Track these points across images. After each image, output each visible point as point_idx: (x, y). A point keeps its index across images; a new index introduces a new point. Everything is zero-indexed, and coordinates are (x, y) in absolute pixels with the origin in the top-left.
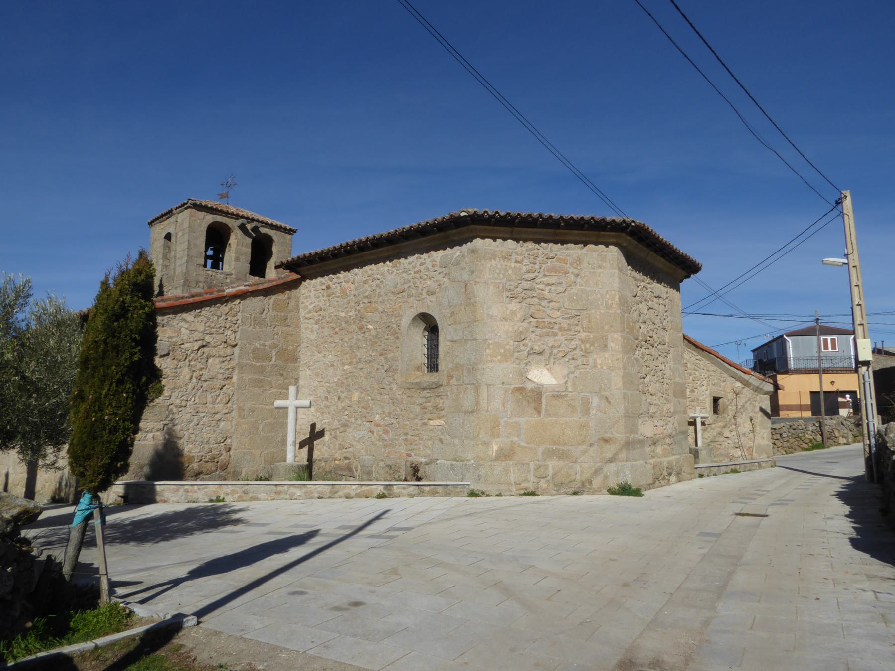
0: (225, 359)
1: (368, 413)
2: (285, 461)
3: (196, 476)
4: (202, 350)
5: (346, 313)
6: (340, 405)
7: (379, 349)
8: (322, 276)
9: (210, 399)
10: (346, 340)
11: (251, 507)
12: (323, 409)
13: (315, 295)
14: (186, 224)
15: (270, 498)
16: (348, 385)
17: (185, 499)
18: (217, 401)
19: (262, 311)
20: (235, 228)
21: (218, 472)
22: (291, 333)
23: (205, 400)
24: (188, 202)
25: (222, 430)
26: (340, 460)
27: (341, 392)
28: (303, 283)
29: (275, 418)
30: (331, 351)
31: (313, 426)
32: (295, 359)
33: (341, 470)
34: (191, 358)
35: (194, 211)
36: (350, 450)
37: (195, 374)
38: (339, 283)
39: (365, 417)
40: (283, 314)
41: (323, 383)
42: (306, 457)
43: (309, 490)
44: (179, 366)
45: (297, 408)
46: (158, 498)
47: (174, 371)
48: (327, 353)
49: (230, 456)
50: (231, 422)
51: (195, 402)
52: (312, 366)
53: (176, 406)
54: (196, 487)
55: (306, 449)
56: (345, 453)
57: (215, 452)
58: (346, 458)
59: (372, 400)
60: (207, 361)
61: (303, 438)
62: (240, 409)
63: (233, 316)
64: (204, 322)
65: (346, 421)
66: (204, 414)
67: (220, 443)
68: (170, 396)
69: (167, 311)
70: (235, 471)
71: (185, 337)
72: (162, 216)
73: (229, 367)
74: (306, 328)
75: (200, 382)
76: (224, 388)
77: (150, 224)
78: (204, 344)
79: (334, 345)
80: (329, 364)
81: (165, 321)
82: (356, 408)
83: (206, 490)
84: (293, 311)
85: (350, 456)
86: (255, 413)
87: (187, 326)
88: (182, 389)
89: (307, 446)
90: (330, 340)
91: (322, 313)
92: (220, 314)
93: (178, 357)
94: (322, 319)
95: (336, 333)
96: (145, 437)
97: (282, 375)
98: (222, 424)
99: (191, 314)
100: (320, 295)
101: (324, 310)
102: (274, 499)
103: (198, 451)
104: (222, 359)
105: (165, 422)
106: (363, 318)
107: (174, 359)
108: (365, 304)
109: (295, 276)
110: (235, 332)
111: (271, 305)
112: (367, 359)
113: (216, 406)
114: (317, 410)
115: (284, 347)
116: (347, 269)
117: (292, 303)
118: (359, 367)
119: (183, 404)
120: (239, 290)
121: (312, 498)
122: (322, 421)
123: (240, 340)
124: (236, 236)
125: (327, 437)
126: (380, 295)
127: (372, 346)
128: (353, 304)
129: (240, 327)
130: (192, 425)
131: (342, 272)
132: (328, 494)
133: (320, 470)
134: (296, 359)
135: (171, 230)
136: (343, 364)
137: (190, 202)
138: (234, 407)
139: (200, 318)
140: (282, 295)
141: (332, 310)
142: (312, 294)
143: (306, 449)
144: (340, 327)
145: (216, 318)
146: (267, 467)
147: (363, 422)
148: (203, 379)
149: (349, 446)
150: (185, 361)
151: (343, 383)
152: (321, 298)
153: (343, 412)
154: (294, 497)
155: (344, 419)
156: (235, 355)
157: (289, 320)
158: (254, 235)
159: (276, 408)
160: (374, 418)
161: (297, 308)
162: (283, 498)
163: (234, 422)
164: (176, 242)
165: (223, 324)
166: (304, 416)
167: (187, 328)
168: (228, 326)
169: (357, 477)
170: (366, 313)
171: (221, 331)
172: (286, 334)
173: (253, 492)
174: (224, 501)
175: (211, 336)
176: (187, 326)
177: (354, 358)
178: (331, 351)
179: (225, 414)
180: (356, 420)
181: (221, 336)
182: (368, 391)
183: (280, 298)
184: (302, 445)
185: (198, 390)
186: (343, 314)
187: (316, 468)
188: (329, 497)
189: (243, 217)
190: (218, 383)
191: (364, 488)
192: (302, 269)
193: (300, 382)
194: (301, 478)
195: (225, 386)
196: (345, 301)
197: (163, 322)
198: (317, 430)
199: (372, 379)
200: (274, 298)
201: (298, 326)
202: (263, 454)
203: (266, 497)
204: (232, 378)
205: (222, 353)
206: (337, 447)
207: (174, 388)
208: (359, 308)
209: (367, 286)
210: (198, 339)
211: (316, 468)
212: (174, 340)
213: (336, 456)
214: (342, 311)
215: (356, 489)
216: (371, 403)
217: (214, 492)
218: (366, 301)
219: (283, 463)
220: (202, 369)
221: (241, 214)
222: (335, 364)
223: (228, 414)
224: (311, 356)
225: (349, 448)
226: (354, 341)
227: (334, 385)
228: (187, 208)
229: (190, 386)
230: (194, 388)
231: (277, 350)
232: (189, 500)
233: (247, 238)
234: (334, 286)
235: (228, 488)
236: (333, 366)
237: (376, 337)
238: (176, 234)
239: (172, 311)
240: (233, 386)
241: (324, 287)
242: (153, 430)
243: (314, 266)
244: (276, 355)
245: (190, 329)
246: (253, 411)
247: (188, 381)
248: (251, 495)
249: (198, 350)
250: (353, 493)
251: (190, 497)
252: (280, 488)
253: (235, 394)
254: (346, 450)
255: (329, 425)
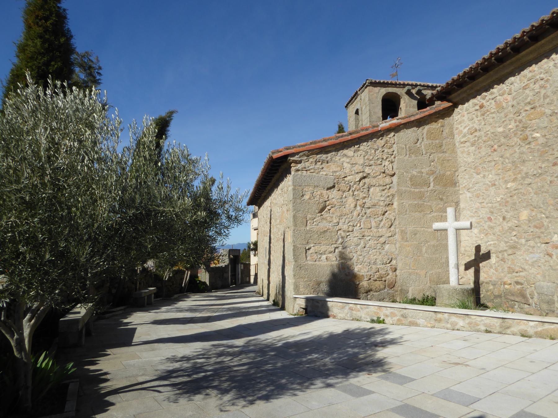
0: (385, 187)
1: (542, 233)
2: (448, 282)
3: (367, 293)
4: (363, 181)
5: (504, 128)
6: (506, 225)
7: (551, 158)
8: (475, 97)
9: (373, 224)
10: (508, 155)
11: (405, 338)
12: (487, 230)
13: (469, 118)
14: (367, 99)
15: (429, 325)
16: (514, 204)
17: (350, 317)
18: (381, 225)
19: (416, 140)
20: (403, 95)
21: (386, 290)
22: (447, 158)
23: (369, 225)
24: (366, 82)
25: (387, 252)
26: (511, 284)
27: (506, 211)
28: (456, 110)
29: (438, 240)
30: (491, 170)
31: (478, 248)
32: (454, 184)
33: (513, 295)
34: (354, 189)
35: (371, 87)
36: (521, 274)
37: (359, 203)
38: (493, 99)
39: (539, 237)
40: (437, 141)
41: (485, 204)
42: (472, 279)
43: (474, 321)
44: (344, 196)
45: (457, 230)
46: (330, 313)
47: (339, 200)
48: (487, 174)
49: (396, 276)
50: (395, 244)
51: (361, 227)
52: (472, 188)
53: (344, 231)
54: (358, 306)
55: (472, 270)
56: (516, 277)
57: (382, 272)
58: (517, 283)
59: (547, 217)
60: (369, 191)
61: (468, 259)
62: (403, 232)
63: (389, 148)
64: (362, 156)
65: (515, 242)
66: (369, 238)
67: (386, 264)
68: (338, 223)
69: (330, 149)
70: (402, 289)
71: (347, 171)
72: (352, 99)
73: (389, 194)
74: (462, 153)
75: (364, 209)
76: (386, 214)
77: (346, 107)
78: (365, 175)
79: (493, 163)
80: (490, 184)
81: (329, 158)
82: (526, 227)
83: (367, 310)
84: (447, 138)
85: (522, 281)
86: (418, 236)
87: (348, 160)
88: (348, 216)
89: (473, 268)
90: (490, 159)
91: (477, 134)
92: (376, 148)
93: (342, 188)
94: (478, 140)
95: (495, 150)
96: (320, 258)
97: (442, 199)
98: (387, 247)
99: (351, 150)
100: (474, 116)
101: (480, 130)
102: (433, 327)
103: (366, 271)
104: (382, 188)
105: (335, 246)
106: (526, 128)
107: (339, 190)
108: (528, 112)
109: (446, 104)
110: (392, 162)
111: (425, 135)
112: (535, 172)
113: (380, 230)
114: (480, 232)
115: (442, 172)
116: (501, 81)
117: (446, 131)
118: (526, 182)
119: (350, 229)
120: (392, 124)
121: (478, 331)
122: (487, 242)
123: (397, 169)
124: (404, 101)
125: (493, 259)
126: (546, 96)
127: (541, 156)
128: (512, 116)
129: (396, 158)
130: (359, 247)
131: (495, 86)
132: (498, 329)
133: (488, 294)
134: (455, 184)
135: (358, 106)
136: (506, 182)
137: (368, 81)
138: (397, 230)
139: (359, 153)
140: (436, 124)
141: (488, 128)
142: (465, 118)
143: (472, 270)
144: (499, 144)
145: (373, 151)
146: (433, 286)
147: (536, 243)
148: (366, 206)
149: (521, 269)
150: (348, 191)
151: (507, 202)
152: (476, 119)
153: (510, 233)
154: (457, 327)
155: (512, 240)
156: (394, 183)
157: (444, 147)
158: (419, 97)
159: (435, 230)
160: (551, 239)
161: (452, 135)
162: (444, 326)
163: (398, 245)
164: (362, 114)
165: (380, 156)
166: (467, 238)
167: (348, 163)
168: (385, 158)
169: (534, 305)
170: (529, 122)
171: (379, 162)
172: (443, 160)
173: (412, 317)
174: (384, 323)
175: (370, 167)
176: (348, 160)
177: (520, 173)
178: (491, 170)
179: (389, 237)
180: (527, 241)
181: (379, 167)
182: (540, 208)
183: (434, 127)
184: (468, 266)
185: (362, 216)
186: (501, 130)
187: (484, 290)
188: (500, 333)
189: (408, 85)
190: (380, 210)
191: (547, 326)
192: (453, 95)
193: (460, 204)
194: (464, 306)
195: (386, 212)
196: (502, 115)
197: (328, 159)
198: (482, 252)
199: (545, 194)
200: (427, 128)
201: (454, 151)
202: (428, 275)
203: (426, 323)
204: (393, 204)
205: (381, 183)
206: (506, 269)
207: (341, 215)
208: (520, 117)
209: (527, 91)
210: (358, 171)
211: (484, 290)
212: (338, 174)
213: (506, 279)
214: (499, 127)
215: (536, 326)
216: (546, 222)
217: (375, 313)
218: (528, 108)
219: (445, 286)
220: (364, 198)
221: (406, 83)
222: (497, 183)
223: (392, 238)
224: (469, 178)
225: (521, 272)
226: (517, 155)
227: (497, 205)
228: (366, 88)
229: (355, 213)
230: (359, 215)
231: (435, 176)
232: (354, 318)
233: (413, 100)
234: (488, 103)
235: (387, 310)
236: (495, 185)
237: (545, 145)
238: (362, 108)
239: (334, 149)
240: (394, 212)
241: (477, 107)
242: (326, 253)
243: (465, 89)
244: (434, 180)
245: (351, 163)
246: (415, 234)
247: (353, 209)
248: (410, 319)
249: (360, 181)
250: (531, 331)
251: (354, 315)
252: (439, 316)
253: (397, 219)
254: (518, 274)
255: (494, 247)
